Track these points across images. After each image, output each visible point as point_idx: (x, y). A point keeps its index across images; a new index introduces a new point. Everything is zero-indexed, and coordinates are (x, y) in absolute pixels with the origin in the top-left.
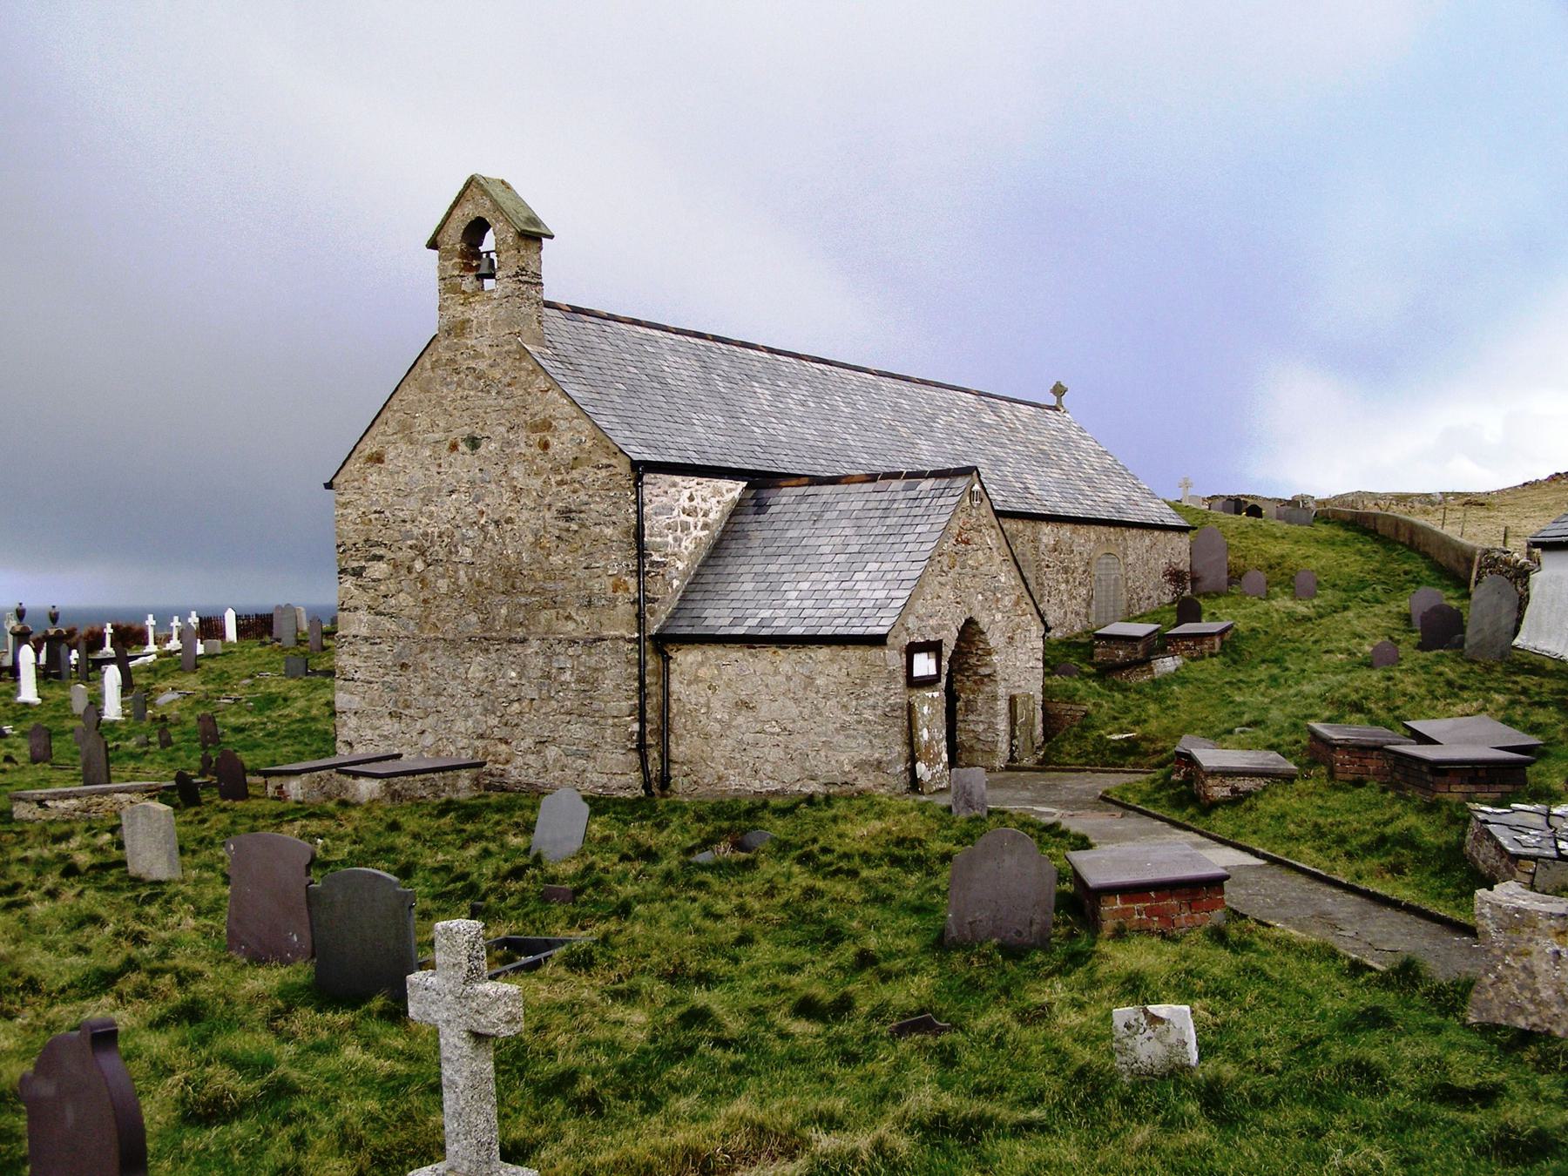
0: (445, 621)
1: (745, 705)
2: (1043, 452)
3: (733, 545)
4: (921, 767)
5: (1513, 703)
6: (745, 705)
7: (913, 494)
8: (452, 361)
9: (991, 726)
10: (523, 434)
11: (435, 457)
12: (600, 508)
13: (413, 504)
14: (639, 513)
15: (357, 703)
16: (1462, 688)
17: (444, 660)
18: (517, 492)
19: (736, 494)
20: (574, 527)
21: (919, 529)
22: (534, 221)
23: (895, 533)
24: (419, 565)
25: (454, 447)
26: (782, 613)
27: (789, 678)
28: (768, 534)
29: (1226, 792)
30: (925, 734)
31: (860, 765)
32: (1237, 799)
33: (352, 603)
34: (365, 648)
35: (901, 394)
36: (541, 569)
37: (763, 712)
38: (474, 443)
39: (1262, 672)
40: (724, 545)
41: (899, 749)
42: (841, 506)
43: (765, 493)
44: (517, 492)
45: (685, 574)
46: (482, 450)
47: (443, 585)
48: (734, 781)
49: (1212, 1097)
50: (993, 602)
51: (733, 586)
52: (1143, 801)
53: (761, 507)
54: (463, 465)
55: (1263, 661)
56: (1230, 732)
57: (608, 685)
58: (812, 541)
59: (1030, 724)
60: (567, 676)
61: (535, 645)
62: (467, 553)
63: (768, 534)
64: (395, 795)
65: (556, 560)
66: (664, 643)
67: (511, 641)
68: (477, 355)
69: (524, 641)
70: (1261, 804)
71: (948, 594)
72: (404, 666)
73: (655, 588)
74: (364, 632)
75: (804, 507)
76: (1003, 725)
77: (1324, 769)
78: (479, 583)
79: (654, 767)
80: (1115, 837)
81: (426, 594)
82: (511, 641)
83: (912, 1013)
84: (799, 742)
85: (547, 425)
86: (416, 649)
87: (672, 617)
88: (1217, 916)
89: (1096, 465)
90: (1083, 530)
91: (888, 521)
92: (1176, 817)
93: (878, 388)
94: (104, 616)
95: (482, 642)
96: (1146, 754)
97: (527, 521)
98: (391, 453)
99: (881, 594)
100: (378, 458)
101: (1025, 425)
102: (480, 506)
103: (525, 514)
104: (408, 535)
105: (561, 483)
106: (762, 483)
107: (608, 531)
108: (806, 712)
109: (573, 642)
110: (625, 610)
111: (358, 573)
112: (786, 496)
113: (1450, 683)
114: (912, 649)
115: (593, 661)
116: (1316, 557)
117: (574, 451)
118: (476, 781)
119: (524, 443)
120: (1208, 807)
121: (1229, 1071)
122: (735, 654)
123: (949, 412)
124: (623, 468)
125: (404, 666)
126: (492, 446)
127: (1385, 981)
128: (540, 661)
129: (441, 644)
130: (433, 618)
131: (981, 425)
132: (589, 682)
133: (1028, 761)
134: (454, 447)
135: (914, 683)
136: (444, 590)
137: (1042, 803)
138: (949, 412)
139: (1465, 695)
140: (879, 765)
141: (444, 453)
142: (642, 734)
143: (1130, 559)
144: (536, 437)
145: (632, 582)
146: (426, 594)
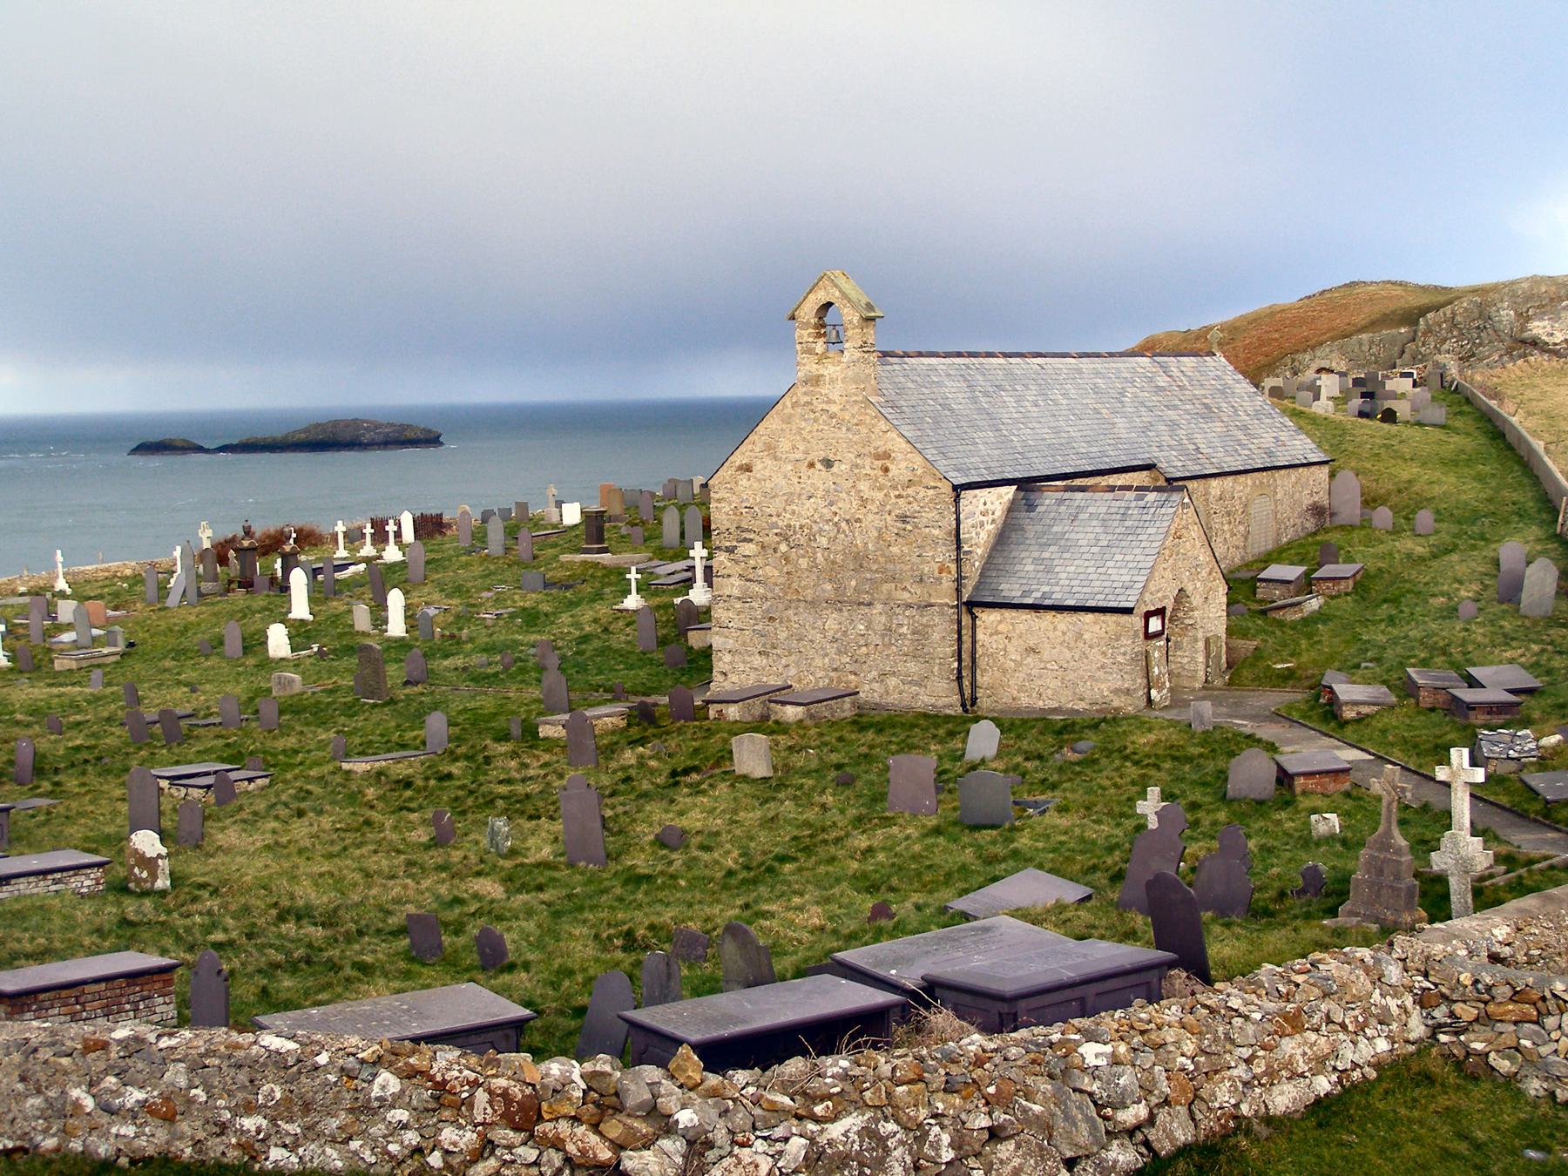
0: (805, 588)
1: (1032, 650)
2: (1206, 406)
3: (1013, 535)
4: (1154, 692)
5: (1543, 651)
6: (1032, 650)
7: (1142, 503)
9: (1193, 659)
10: (868, 461)
11: (796, 471)
12: (930, 515)
13: (778, 503)
14: (958, 520)
15: (730, 644)
16: (1513, 639)
17: (805, 616)
18: (864, 502)
19: (1010, 496)
20: (909, 527)
21: (1150, 531)
23: (1132, 532)
24: (783, 548)
25: (812, 465)
26: (1057, 589)
27: (1064, 633)
28: (1039, 528)
29: (1353, 714)
30: (1156, 670)
31: (1116, 691)
32: (1360, 719)
33: (726, 572)
34: (738, 605)
35: (1097, 373)
36: (883, 555)
37: (1046, 655)
38: (828, 464)
39: (1385, 610)
40: (1005, 537)
41: (1141, 681)
42: (1090, 510)
43: (1032, 496)
44: (864, 502)
45: (982, 557)
46: (835, 469)
47: (803, 563)
48: (1024, 701)
49: (1344, 842)
50: (1194, 575)
51: (1018, 567)
52: (1304, 717)
53: (1031, 507)
55: (1385, 601)
56: (1358, 666)
57: (936, 636)
58: (1073, 536)
59: (1219, 656)
60: (904, 630)
61: (879, 607)
62: (824, 541)
63: (1039, 528)
64: (812, 716)
65: (895, 550)
66: (972, 606)
67: (860, 604)
68: (829, 402)
69: (870, 604)
70: (1374, 723)
71: (1168, 574)
72: (771, 619)
73: (966, 569)
74: (736, 592)
75: (1063, 508)
76: (1201, 658)
77: (1412, 701)
78: (834, 562)
79: (967, 692)
80: (1289, 742)
81: (789, 568)
82: (860, 604)
84: (1071, 676)
85: (887, 456)
86: (781, 607)
87: (976, 588)
88: (1347, 786)
90: (1241, 478)
91: (1127, 524)
92: (1324, 729)
93: (1079, 371)
95: (837, 603)
96: (1300, 679)
97: (871, 521)
98: (758, 466)
99: (1127, 578)
100: (748, 468)
101: (1190, 379)
102: (834, 509)
103: (871, 517)
105: (899, 496)
106: (1027, 485)
107: (936, 532)
108: (1077, 657)
109: (909, 606)
110: (948, 583)
112: (1048, 499)
113: (1505, 635)
114: (1148, 615)
115: (924, 621)
116: (1439, 482)
118: (853, 703)
119: (869, 466)
120: (1344, 724)
121: (1349, 835)
122: (1025, 616)
124: (946, 489)
125: (771, 619)
126: (843, 467)
127: (1416, 811)
128: (883, 619)
129: (802, 605)
130: (795, 585)
132: (921, 633)
133: (1218, 683)
134: (812, 465)
135: (1148, 636)
136: (804, 566)
137: (1237, 717)
139: (1514, 644)
140: (1128, 692)
141: (804, 467)
142: (959, 670)
143: (1279, 496)
144: (879, 463)
145: (953, 567)
146: (789, 568)
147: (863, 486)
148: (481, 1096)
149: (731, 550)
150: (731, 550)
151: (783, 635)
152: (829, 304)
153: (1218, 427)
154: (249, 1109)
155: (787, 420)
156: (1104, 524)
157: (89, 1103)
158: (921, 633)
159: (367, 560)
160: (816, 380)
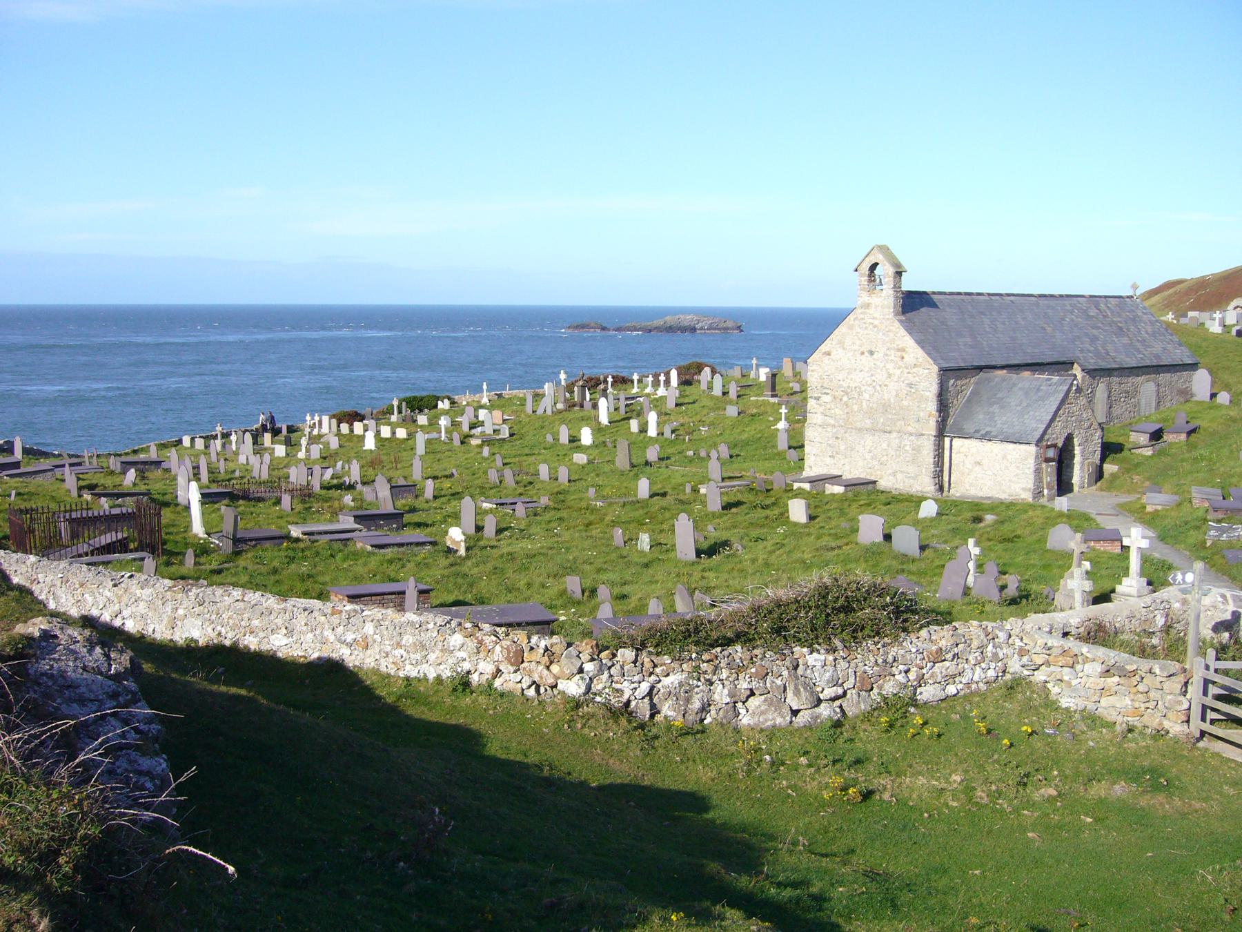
2: (1121, 328)
18: (890, 376)
23: (1042, 399)
24: (845, 399)
35: (1048, 307)
38: (871, 353)
44: (890, 376)
46: (875, 356)
47: (855, 408)
54: (866, 360)
61: (895, 434)
65: (905, 403)
83: (103, 563)
89: (1150, 330)
95: (872, 430)
104: (841, 386)
109: (911, 434)
117: (914, 361)
119: (893, 355)
123: (1072, 312)
131: (1089, 317)
132: (917, 450)
138: (1072, 312)
147: (890, 366)
148: (498, 648)
149: (817, 399)
150: (817, 399)
151: (842, 447)
152: (876, 264)
153: (1125, 340)
154: (399, 645)
155: (851, 328)
156: (1026, 394)
157: (332, 638)
158: (917, 450)
159: (648, 395)
160: (868, 306)
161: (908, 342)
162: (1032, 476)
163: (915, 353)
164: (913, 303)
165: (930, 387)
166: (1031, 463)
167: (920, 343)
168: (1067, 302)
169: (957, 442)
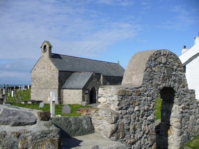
2: (114, 69)
8: (42, 59)
13: (38, 74)
18: (48, 73)
22: (51, 45)
24: (39, 81)
25: (42, 68)
38: (44, 68)
44: (48, 73)
54: (43, 70)
94: (15, 85)
97: (49, 76)
111: (33, 81)
153: (115, 71)
161: (52, 64)
162: (81, 98)
163: (53, 67)
164: (55, 57)
165: (57, 76)
166: (81, 94)
167: (55, 65)
168: (101, 62)
169: (64, 90)
